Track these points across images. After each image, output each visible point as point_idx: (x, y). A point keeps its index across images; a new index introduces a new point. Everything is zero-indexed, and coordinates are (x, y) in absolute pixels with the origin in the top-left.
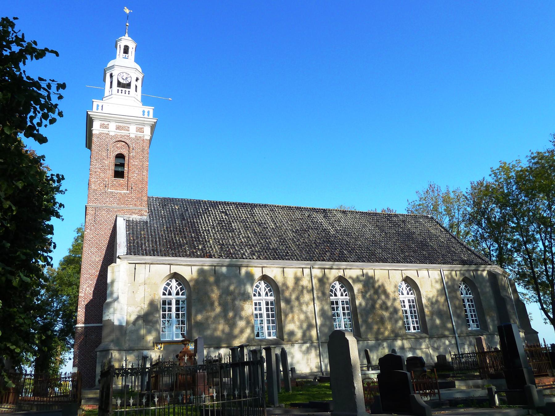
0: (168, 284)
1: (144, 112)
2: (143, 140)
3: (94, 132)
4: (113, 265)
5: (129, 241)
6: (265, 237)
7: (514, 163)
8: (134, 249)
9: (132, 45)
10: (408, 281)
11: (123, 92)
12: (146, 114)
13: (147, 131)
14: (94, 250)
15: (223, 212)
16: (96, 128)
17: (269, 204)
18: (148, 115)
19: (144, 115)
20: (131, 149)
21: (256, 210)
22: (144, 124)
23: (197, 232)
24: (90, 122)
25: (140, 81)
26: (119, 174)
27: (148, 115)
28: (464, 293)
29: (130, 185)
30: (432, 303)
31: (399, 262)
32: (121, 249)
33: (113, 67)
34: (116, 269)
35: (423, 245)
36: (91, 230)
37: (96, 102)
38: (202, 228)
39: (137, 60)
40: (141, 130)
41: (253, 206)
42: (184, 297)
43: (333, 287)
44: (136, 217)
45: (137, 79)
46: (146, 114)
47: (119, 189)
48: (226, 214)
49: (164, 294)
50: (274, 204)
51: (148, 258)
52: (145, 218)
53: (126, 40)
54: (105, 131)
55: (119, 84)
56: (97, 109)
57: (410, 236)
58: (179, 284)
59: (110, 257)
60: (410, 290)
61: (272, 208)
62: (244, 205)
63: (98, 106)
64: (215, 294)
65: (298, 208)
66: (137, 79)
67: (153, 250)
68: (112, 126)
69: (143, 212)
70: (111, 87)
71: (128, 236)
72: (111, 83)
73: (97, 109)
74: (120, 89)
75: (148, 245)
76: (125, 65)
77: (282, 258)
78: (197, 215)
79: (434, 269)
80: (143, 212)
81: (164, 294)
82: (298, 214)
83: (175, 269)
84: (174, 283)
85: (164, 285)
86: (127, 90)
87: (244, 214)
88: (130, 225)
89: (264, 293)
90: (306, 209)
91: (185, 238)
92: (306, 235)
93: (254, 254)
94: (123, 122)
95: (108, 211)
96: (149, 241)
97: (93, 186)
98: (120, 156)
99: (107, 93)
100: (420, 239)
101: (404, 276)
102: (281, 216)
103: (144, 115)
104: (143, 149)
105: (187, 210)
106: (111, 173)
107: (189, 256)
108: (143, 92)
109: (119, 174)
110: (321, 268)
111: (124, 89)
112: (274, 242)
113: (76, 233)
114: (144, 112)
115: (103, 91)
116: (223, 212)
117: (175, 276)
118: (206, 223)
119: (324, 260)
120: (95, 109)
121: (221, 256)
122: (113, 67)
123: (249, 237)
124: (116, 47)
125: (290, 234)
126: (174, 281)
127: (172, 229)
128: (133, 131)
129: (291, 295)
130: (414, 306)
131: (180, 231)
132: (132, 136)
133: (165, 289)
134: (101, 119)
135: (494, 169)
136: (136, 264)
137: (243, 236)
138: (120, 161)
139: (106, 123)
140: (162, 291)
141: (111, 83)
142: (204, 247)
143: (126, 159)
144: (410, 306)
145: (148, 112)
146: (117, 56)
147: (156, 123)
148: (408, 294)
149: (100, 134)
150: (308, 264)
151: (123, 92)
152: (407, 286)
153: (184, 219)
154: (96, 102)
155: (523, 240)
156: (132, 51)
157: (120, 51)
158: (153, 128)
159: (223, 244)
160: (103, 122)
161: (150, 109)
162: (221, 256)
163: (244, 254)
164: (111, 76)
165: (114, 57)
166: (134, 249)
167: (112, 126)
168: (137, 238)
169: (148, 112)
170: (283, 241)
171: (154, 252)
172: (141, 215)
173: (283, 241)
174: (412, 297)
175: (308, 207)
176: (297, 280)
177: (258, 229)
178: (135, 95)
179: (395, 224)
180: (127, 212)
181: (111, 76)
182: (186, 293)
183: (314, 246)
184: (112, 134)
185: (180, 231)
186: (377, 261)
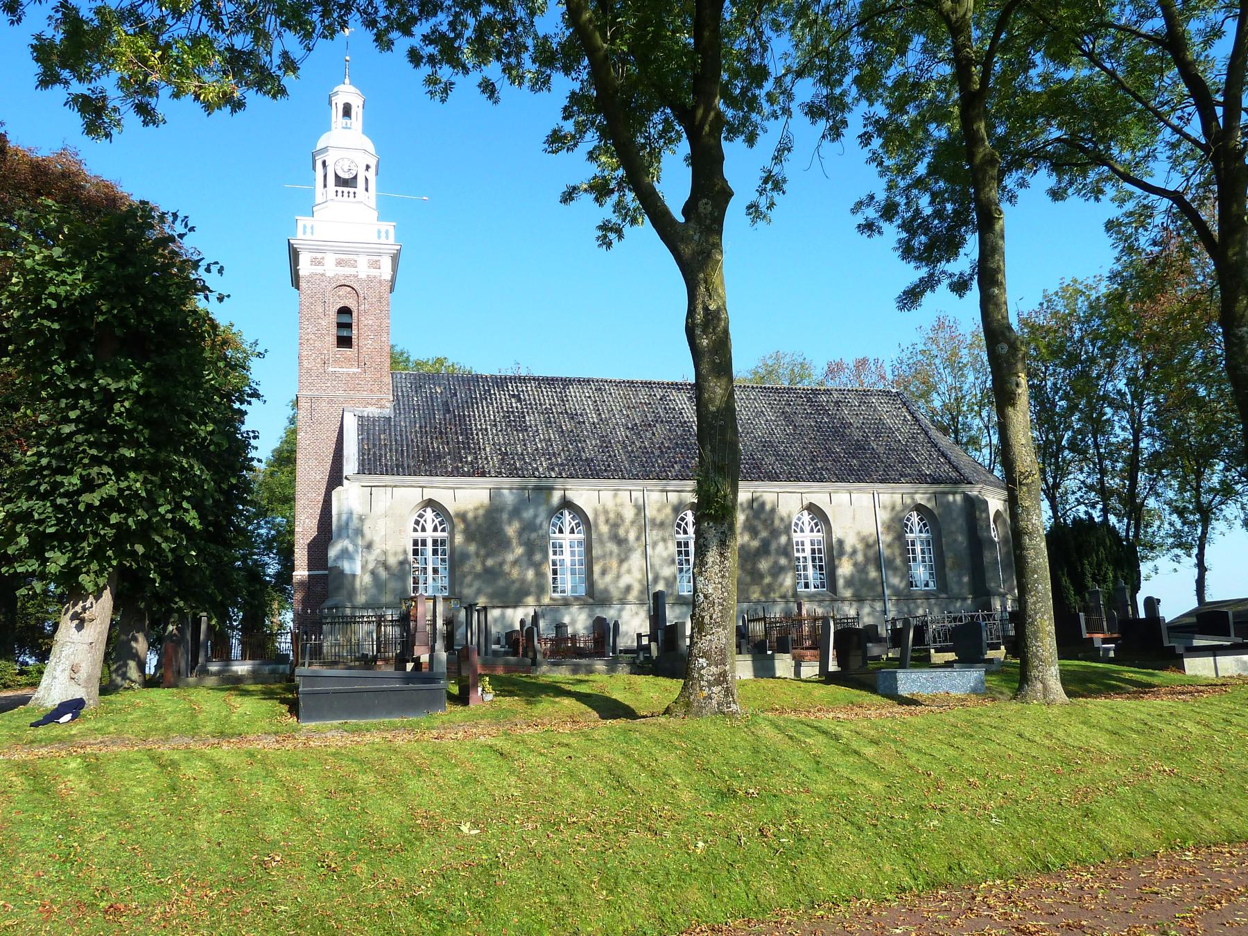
0: (421, 516)
1: (379, 232)
2: (380, 282)
3: (301, 273)
4: (339, 488)
5: (361, 452)
6: (576, 439)
7: (1090, 282)
8: (369, 465)
9: (357, 102)
10: (812, 509)
11: (346, 194)
12: (383, 235)
13: (386, 263)
14: (313, 463)
15: (514, 396)
16: (305, 268)
17: (595, 377)
18: (387, 238)
19: (379, 237)
20: (361, 298)
21: (572, 390)
22: (380, 254)
23: (467, 433)
24: (294, 255)
25: (373, 170)
26: (344, 342)
27: (387, 238)
28: (917, 535)
29: (361, 358)
30: (868, 546)
31: (798, 479)
32: (350, 465)
33: (325, 149)
34: (343, 496)
35: (860, 447)
36: (306, 432)
37: (303, 221)
38: (476, 425)
39: (367, 130)
40: (376, 265)
41: (567, 382)
42: (445, 534)
43: (682, 519)
44: (372, 411)
45: (368, 167)
46: (383, 235)
47: (344, 365)
48: (519, 400)
49: (415, 530)
50: (604, 378)
51: (388, 479)
52: (388, 411)
53: (347, 93)
54: (319, 270)
55: (341, 182)
56: (305, 233)
57: (839, 431)
58: (437, 515)
59: (336, 478)
60: (816, 525)
61: (599, 385)
62: (550, 381)
63: (305, 227)
64: (511, 530)
65: (648, 385)
66: (368, 167)
67: (397, 466)
68: (330, 259)
69: (383, 402)
70: (325, 186)
71: (361, 442)
72: (325, 176)
73: (305, 233)
74: (340, 189)
75: (390, 458)
76: (347, 144)
77: (597, 475)
78: (470, 402)
79: (860, 490)
80: (383, 402)
81: (415, 530)
82: (643, 395)
83: (429, 494)
84: (429, 514)
85: (415, 517)
86: (351, 190)
87: (548, 397)
88: (365, 425)
89: (568, 529)
90: (661, 385)
91: (448, 443)
92: (649, 435)
93: (553, 469)
94: (346, 254)
95: (331, 401)
96: (390, 453)
97: (305, 364)
98: (345, 311)
99: (319, 198)
100: (857, 435)
101: (805, 503)
102: (614, 401)
103: (379, 237)
104: (381, 297)
105: (455, 394)
106: (333, 340)
107: (451, 474)
108: (379, 187)
109: (344, 342)
110: (662, 491)
111: (346, 189)
112: (590, 448)
113: (289, 408)
114: (379, 232)
115: (312, 193)
116: (514, 396)
117: (430, 503)
118: (484, 417)
119: (667, 478)
120: (300, 235)
121: (500, 473)
122: (325, 149)
123: (550, 440)
124: (330, 103)
125: (621, 433)
126: (429, 510)
127: (436, 424)
128: (363, 269)
129: (627, 532)
130: (820, 551)
131: (441, 433)
132: (363, 276)
133: (417, 523)
134: (311, 251)
135: (1051, 292)
136: (454, 489)
137: (543, 436)
138: (345, 319)
139: (319, 256)
140: (413, 525)
141: (325, 176)
142: (476, 458)
143: (355, 314)
144: (813, 551)
145: (387, 232)
146: (333, 126)
147: (399, 251)
148: (812, 531)
149: (312, 275)
150: (656, 485)
151: (346, 194)
152: (812, 519)
153: (449, 411)
154: (303, 221)
155: (132, 546)
156: (357, 111)
157: (336, 114)
158: (395, 259)
159: (506, 454)
160: (314, 255)
161: (389, 227)
162: (500, 473)
163: (537, 469)
164: (324, 163)
165: (326, 127)
166: (369, 465)
167: (330, 259)
168: (374, 445)
169: (387, 232)
170: (605, 445)
171: (399, 469)
172: (381, 406)
173: (605, 445)
174: (818, 536)
175: (666, 381)
176: (640, 509)
177: (567, 425)
178: (365, 199)
179: (821, 410)
180: (362, 397)
181: (324, 163)
182: (448, 529)
183: (657, 452)
184: (330, 274)
185: (441, 433)
186: (759, 479)
